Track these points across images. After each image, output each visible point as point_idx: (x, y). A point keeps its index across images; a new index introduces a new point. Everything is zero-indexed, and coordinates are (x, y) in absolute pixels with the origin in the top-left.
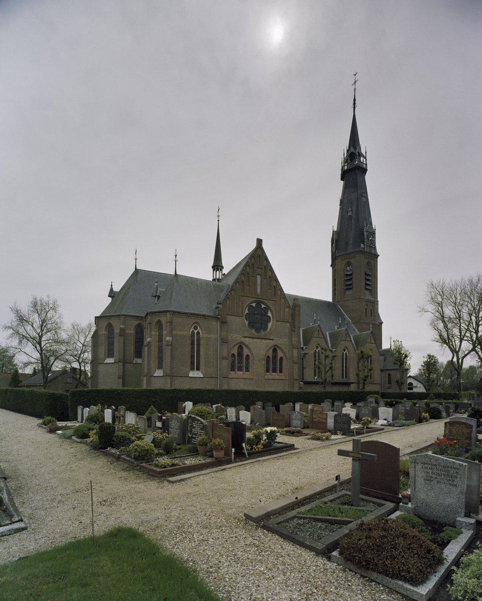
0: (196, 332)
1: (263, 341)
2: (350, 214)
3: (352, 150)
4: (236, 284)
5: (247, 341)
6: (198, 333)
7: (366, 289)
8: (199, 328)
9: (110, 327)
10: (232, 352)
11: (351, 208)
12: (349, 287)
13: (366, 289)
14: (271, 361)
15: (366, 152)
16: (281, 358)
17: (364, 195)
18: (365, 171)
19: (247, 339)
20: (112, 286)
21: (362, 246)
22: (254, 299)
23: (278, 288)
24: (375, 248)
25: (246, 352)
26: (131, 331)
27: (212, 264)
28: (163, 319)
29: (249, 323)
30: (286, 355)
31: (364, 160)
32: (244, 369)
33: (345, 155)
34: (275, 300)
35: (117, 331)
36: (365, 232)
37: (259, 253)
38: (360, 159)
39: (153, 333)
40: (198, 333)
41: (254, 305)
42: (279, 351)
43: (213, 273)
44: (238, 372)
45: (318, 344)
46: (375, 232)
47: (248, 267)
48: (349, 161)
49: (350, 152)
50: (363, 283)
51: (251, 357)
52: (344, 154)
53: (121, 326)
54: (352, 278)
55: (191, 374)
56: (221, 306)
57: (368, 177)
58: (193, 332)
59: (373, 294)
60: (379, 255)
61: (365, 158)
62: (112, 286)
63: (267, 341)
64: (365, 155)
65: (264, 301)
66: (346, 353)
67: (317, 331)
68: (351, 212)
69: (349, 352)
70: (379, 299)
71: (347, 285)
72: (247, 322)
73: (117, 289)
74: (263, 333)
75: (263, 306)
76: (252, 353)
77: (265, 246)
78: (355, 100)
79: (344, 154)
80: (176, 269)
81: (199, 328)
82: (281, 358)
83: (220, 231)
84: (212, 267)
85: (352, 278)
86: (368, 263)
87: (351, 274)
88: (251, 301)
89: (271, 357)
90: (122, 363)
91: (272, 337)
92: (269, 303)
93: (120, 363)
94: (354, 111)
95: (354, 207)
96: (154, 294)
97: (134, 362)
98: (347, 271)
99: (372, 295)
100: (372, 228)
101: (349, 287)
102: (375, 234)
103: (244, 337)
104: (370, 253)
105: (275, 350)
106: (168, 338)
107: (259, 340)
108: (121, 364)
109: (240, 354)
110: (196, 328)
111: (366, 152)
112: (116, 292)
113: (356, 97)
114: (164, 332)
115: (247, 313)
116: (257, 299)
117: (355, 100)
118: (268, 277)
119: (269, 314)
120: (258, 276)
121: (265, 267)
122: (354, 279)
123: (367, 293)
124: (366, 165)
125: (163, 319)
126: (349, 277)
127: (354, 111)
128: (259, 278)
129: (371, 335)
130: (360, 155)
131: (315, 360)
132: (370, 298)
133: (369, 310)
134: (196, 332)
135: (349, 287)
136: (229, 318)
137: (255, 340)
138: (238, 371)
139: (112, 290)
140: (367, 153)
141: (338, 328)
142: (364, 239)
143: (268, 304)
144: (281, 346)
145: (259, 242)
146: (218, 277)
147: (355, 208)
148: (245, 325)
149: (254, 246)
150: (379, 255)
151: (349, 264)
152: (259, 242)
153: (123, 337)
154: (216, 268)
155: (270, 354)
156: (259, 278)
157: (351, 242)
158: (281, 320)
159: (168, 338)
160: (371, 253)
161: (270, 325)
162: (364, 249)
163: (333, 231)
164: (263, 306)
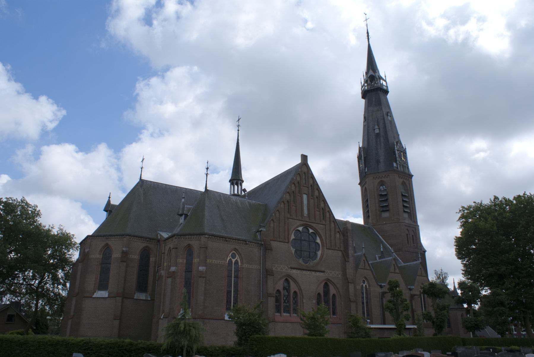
0: (234, 260)
1: (313, 273)
2: (377, 131)
3: (371, 73)
4: (281, 204)
5: (294, 273)
6: (236, 262)
7: (405, 212)
8: (237, 256)
9: (107, 250)
10: (277, 288)
11: (378, 125)
12: (385, 209)
13: (405, 212)
14: (323, 299)
15: (385, 76)
16: (295, 292)
17: (389, 114)
19: (294, 271)
20: (109, 197)
21: (395, 165)
22: (302, 222)
23: (327, 209)
25: (293, 287)
26: (136, 257)
27: (229, 177)
28: (195, 243)
29: (296, 252)
30: (339, 292)
32: (282, 309)
33: (365, 78)
34: (324, 223)
35: (116, 255)
37: (305, 170)
38: (380, 81)
39: (180, 261)
40: (236, 262)
41: (300, 229)
42: (331, 287)
43: (231, 188)
44: (285, 314)
45: (365, 278)
46: (406, 151)
47: (293, 185)
48: (369, 82)
49: (369, 75)
50: (401, 204)
51: (299, 295)
53: (124, 249)
54: (387, 200)
56: (264, 229)
58: (230, 261)
59: (413, 218)
60: (413, 176)
61: (385, 81)
62: (109, 197)
63: (318, 274)
64: (384, 78)
65: (312, 224)
66: (366, 285)
67: (393, 265)
68: (378, 130)
69: (369, 286)
71: (383, 207)
72: (293, 250)
74: (311, 263)
75: (311, 231)
76: (300, 289)
78: (368, 33)
80: (206, 184)
81: (237, 256)
82: (334, 295)
83: (240, 142)
84: (230, 181)
85: (387, 200)
86: (404, 184)
87: (386, 195)
88: (298, 224)
89: (322, 294)
90: (121, 298)
91: (323, 269)
92: (319, 227)
93: (118, 298)
96: (180, 212)
97: (135, 298)
98: (381, 190)
99: (411, 219)
100: (403, 147)
101: (385, 209)
103: (292, 268)
104: (404, 173)
105: (326, 285)
106: (201, 268)
107: (309, 272)
108: (119, 299)
109: (287, 289)
110: (233, 256)
111: (385, 76)
112: (114, 206)
113: (368, 31)
114: (196, 260)
115: (294, 239)
116: (304, 222)
117: (368, 33)
118: (315, 197)
119: (318, 241)
120: (304, 195)
123: (406, 215)
124: (387, 87)
125: (195, 243)
126: (384, 197)
128: (305, 197)
129: (421, 266)
130: (380, 78)
131: (422, 310)
132: (410, 222)
133: (411, 236)
134: (234, 260)
135: (385, 209)
136: (274, 244)
137: (304, 272)
138: (284, 312)
139: (109, 202)
140: (386, 77)
141: (380, 258)
143: (317, 228)
144: (333, 280)
145: (304, 158)
146: (236, 192)
148: (292, 253)
149: (298, 161)
150: (413, 176)
151: (382, 183)
153: (125, 264)
154: (235, 182)
155: (321, 290)
156: (305, 197)
157: (382, 160)
158: (332, 248)
159: (201, 268)
160: (405, 173)
161: (319, 253)
162: (397, 168)
164: (311, 231)
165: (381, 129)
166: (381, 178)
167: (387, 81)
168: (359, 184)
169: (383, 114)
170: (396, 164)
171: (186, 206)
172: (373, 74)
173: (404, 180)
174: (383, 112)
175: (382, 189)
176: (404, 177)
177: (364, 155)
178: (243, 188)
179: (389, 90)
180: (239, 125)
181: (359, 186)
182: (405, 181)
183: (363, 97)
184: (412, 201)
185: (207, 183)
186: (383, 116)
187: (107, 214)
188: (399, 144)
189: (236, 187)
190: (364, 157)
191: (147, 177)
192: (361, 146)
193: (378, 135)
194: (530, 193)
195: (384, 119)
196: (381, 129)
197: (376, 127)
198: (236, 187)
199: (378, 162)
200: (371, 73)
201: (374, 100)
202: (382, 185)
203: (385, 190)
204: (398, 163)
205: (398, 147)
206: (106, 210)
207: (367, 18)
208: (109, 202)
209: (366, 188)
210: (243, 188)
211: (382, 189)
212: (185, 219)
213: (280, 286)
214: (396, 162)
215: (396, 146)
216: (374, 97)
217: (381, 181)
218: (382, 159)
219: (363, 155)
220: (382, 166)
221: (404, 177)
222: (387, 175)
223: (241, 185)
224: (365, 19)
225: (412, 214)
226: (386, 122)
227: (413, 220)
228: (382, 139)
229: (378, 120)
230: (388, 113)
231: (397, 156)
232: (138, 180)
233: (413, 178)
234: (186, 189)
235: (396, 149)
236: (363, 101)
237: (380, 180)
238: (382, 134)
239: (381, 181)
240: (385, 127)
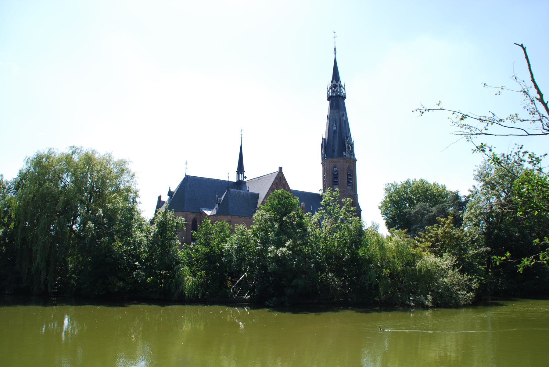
2: (335, 128)
17: (344, 116)
18: (344, 98)
21: (344, 154)
24: (354, 155)
31: (344, 90)
33: (330, 85)
36: (346, 144)
43: (237, 176)
46: (353, 143)
49: (333, 84)
52: (329, 85)
55: (358, 286)
57: (346, 101)
59: (354, 189)
60: (357, 160)
61: (344, 89)
64: (344, 87)
68: (335, 127)
70: (358, 193)
73: (173, 189)
77: (284, 171)
78: (335, 49)
79: (329, 85)
83: (242, 145)
85: (337, 177)
94: (335, 56)
95: (338, 124)
100: (351, 141)
102: (353, 145)
117: (335, 49)
121: (284, 184)
122: (339, 178)
124: (345, 94)
127: (335, 56)
130: (340, 86)
135: (335, 183)
139: (170, 190)
142: (346, 149)
145: (281, 169)
147: (338, 125)
152: (281, 169)
157: (336, 150)
162: (346, 156)
163: (323, 139)
165: (338, 127)
166: (335, 162)
167: (345, 89)
168: (321, 163)
169: (340, 116)
170: (345, 153)
171: (218, 198)
174: (340, 114)
175: (335, 170)
176: (350, 162)
177: (325, 145)
178: (244, 176)
180: (242, 135)
181: (321, 165)
184: (354, 178)
186: (340, 118)
187: (169, 197)
188: (348, 139)
189: (240, 174)
190: (325, 146)
191: (189, 174)
193: (335, 131)
194: (548, 102)
195: (340, 119)
196: (338, 127)
197: (335, 125)
198: (240, 174)
199: (333, 151)
200: (335, 82)
201: (335, 104)
202: (335, 167)
203: (337, 171)
204: (347, 152)
205: (348, 141)
206: (169, 195)
207: (336, 36)
208: (170, 190)
209: (325, 168)
210: (244, 176)
211: (335, 170)
212: (218, 205)
214: (345, 152)
215: (346, 141)
216: (335, 102)
217: (335, 164)
218: (336, 149)
219: (324, 145)
220: (336, 153)
221: (350, 162)
222: (338, 161)
223: (243, 174)
224: (334, 36)
225: (354, 187)
226: (341, 122)
227: (354, 191)
228: (337, 134)
229: (336, 120)
230: (344, 114)
231: (346, 147)
232: (185, 176)
234: (211, 179)
235: (346, 142)
238: (338, 131)
239: (335, 164)
240: (340, 126)
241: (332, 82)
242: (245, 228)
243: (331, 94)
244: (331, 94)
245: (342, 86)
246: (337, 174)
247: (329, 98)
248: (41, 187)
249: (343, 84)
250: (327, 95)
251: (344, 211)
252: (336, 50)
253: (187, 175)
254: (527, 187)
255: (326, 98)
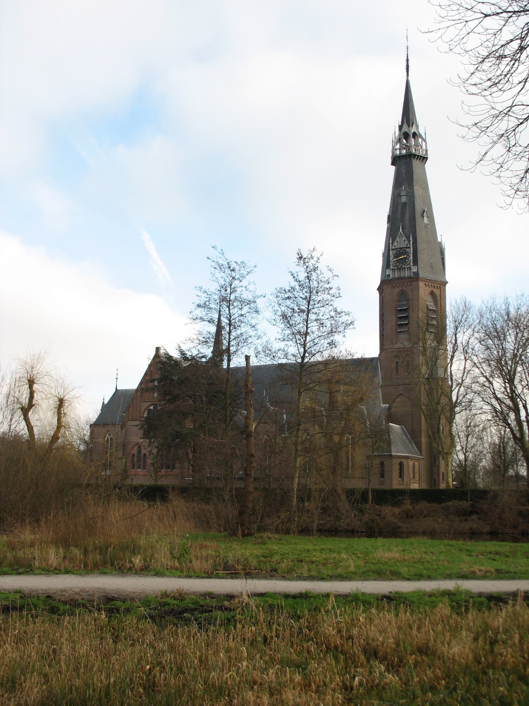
15: (425, 134)
18: (424, 159)
31: (424, 143)
41: (152, 408)
52: (395, 133)
61: (424, 140)
64: (424, 136)
79: (395, 133)
111: (425, 134)
124: (426, 151)
167: (427, 141)
172: (407, 131)
173: (433, 289)
179: (429, 156)
181: (377, 292)
182: (435, 291)
183: (393, 164)
185: (410, 65)
192: (106, 402)
213: (135, 451)
232: (115, 390)
233: (447, 286)
236: (393, 168)
237: (401, 288)
241: (401, 127)
242: (332, 690)
243: (398, 150)
244: (398, 152)
245: (420, 136)
246: (408, 316)
247: (396, 160)
248: (353, 639)
249: (421, 131)
250: (391, 155)
251: (296, 629)
252: (419, 256)
253: (118, 388)
254: (457, 698)
255: (390, 161)
